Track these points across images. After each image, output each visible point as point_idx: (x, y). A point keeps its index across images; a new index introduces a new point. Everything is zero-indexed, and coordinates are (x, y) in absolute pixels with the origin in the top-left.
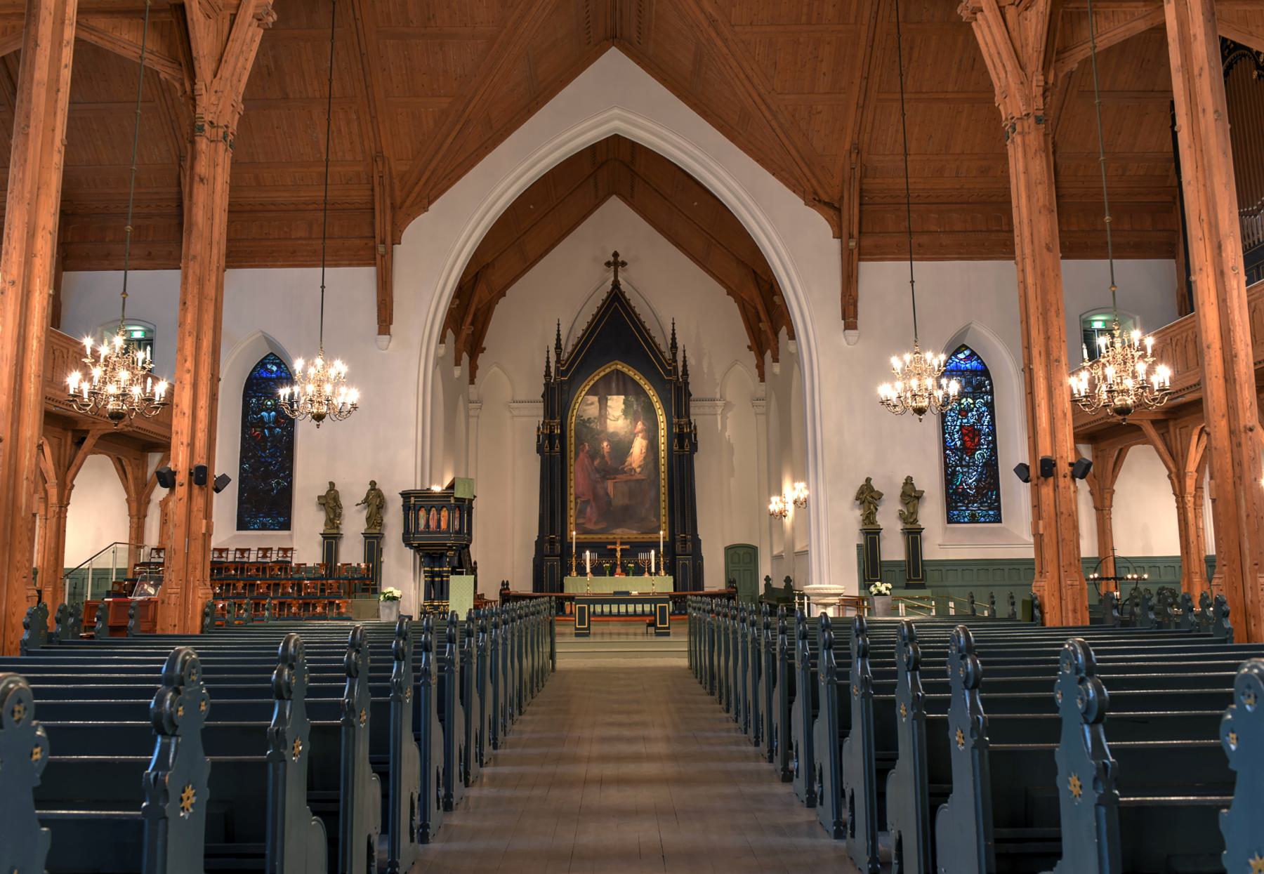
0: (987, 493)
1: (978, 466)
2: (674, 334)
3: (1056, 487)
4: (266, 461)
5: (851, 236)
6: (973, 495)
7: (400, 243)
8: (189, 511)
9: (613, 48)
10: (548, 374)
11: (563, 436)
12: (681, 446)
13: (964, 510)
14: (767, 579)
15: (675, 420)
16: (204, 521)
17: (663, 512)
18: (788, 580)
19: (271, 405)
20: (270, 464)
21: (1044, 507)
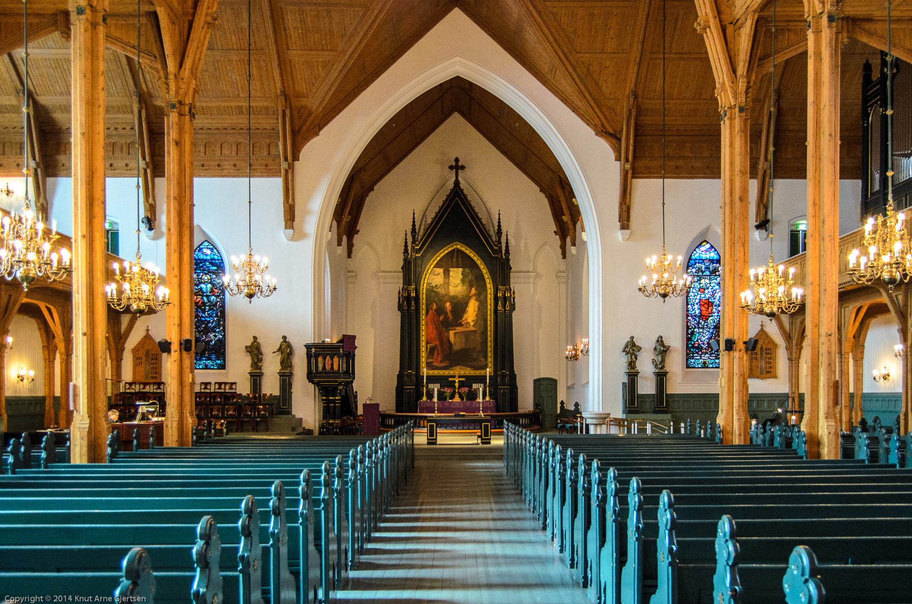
2: (499, 222)
4: (206, 320)
6: (706, 349)
7: (298, 160)
10: (406, 251)
11: (417, 298)
14: (562, 403)
16: (191, 375)
17: (489, 354)
18: (577, 405)
20: (209, 322)
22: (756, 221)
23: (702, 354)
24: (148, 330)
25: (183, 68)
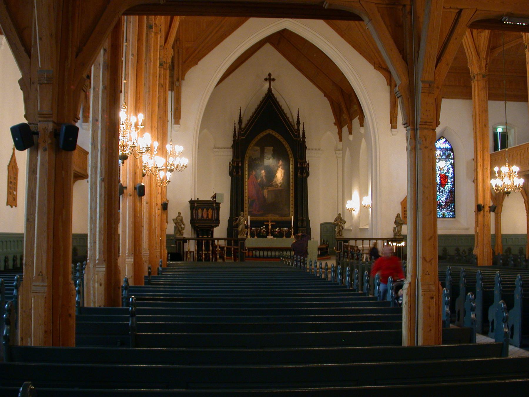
0: (450, 205)
1: (446, 193)
2: (298, 117)
3: (484, 216)
6: (444, 206)
10: (235, 135)
13: (440, 212)
21: (479, 222)
23: (442, 208)
25: (167, 43)
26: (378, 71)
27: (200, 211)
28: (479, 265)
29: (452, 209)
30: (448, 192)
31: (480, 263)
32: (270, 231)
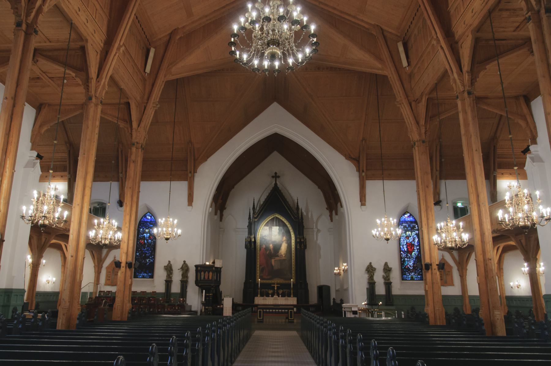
1: (413, 258)
5: (363, 171)
6: (412, 270)
8: (125, 276)
9: (275, 102)
10: (250, 218)
12: (300, 246)
14: (334, 299)
15: (298, 236)
16: (130, 280)
19: (148, 231)
20: (147, 253)
22: (434, 201)
23: (410, 272)
24: (115, 257)
26: (348, 161)
27: (202, 273)
28: (431, 324)
29: (419, 273)
30: (415, 258)
31: (432, 322)
32: (276, 292)
